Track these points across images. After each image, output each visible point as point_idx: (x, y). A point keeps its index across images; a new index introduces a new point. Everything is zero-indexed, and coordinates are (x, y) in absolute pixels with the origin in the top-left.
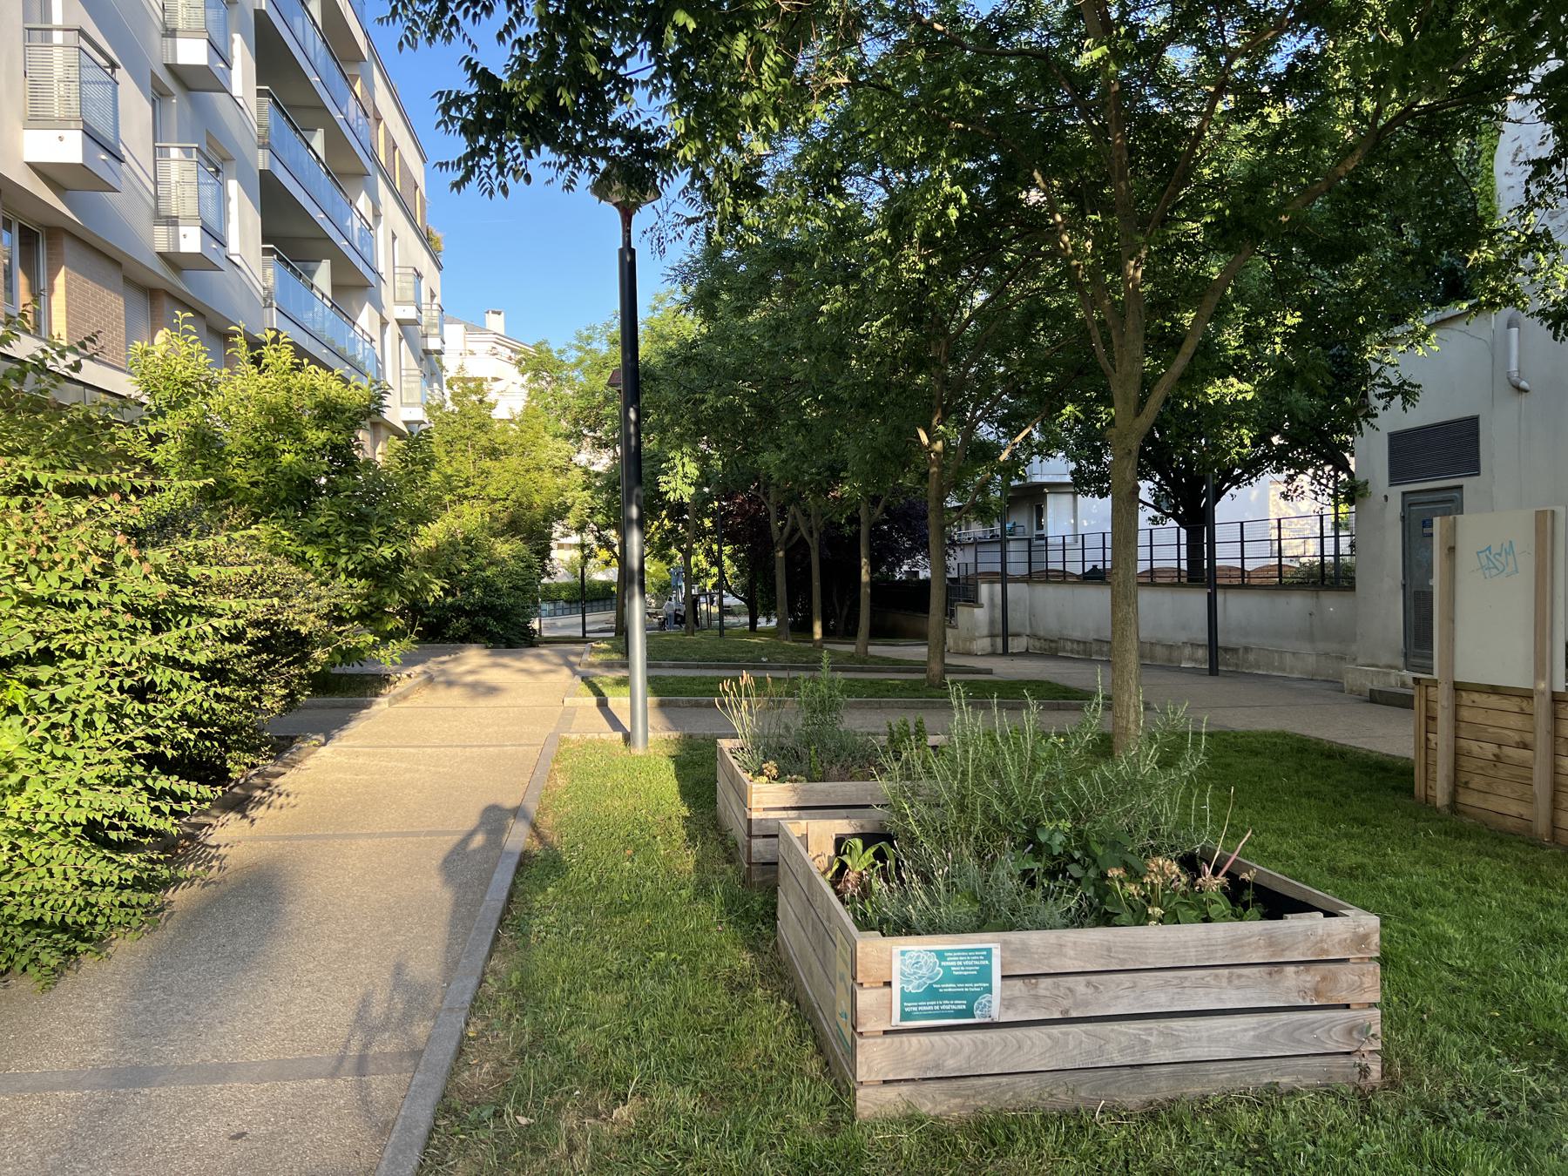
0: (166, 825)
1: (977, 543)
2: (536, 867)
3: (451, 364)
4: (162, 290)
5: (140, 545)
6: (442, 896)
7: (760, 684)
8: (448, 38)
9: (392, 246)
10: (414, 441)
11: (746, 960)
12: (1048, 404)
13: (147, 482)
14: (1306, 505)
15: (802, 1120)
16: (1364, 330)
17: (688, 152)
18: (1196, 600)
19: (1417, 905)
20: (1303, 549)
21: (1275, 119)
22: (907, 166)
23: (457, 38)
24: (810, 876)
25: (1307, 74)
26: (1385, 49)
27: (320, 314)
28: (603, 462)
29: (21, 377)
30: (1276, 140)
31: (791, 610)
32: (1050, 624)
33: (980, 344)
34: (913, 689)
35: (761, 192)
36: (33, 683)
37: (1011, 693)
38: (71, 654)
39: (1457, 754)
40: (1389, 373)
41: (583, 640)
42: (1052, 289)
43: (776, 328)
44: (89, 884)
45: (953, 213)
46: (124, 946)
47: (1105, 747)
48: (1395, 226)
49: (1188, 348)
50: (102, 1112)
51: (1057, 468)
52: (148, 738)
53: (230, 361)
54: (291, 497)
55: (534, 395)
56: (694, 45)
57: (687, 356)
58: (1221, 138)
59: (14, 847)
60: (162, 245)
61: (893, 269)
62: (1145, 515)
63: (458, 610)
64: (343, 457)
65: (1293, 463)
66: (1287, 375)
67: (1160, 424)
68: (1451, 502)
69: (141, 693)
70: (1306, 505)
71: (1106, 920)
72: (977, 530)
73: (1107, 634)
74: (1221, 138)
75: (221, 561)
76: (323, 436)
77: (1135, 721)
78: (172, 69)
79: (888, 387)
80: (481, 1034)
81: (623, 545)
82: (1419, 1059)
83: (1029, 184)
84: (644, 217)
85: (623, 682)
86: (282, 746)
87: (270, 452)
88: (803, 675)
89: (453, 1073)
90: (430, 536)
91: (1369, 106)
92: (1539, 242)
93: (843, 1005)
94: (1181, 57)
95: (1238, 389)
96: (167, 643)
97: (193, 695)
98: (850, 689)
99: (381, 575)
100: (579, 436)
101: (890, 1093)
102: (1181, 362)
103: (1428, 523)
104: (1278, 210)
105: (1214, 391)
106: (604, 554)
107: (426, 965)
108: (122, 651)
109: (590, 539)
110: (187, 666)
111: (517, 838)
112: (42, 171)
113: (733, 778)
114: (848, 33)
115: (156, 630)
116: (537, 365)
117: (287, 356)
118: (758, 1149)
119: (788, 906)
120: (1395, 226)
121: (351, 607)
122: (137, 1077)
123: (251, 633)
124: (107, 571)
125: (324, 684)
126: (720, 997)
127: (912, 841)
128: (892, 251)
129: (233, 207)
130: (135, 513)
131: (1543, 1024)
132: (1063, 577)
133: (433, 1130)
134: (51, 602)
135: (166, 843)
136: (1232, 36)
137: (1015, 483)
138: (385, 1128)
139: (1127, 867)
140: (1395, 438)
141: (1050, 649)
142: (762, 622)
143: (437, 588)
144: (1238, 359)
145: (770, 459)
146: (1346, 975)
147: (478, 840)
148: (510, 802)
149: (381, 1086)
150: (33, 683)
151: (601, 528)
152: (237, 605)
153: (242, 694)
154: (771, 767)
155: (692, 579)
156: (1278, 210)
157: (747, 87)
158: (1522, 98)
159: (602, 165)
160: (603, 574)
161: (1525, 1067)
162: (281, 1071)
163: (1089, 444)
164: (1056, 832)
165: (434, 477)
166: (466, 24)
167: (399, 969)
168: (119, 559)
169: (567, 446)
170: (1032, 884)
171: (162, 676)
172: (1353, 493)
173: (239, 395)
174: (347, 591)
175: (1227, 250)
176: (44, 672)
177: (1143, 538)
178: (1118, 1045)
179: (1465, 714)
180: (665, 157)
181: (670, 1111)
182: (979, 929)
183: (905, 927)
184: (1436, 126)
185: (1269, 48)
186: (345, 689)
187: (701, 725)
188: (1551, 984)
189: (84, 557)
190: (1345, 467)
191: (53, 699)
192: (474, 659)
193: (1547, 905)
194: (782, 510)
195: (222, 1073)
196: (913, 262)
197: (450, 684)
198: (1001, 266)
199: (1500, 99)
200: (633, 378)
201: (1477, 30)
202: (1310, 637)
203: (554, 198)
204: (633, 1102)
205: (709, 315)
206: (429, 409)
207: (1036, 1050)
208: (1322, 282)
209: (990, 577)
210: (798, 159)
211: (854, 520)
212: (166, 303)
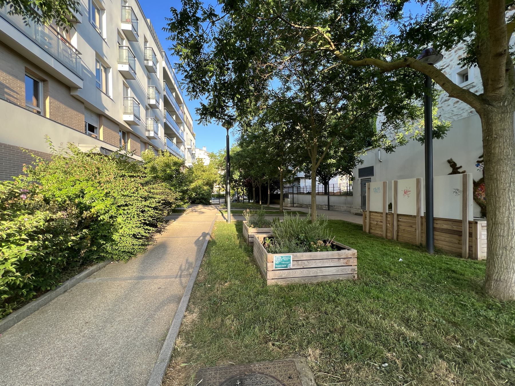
0: (147, 235)
1: (288, 187)
2: (211, 243)
3: (197, 156)
4: (147, 143)
5: (143, 186)
6: (195, 248)
7: (250, 211)
8: (197, 99)
9: (186, 135)
10: (190, 169)
11: (248, 258)
12: (300, 163)
13: (144, 175)
14: (345, 181)
15: (258, 285)
16: (354, 151)
17: (238, 119)
18: (326, 197)
19: (363, 249)
20: (344, 189)
21: (339, 115)
22: (276, 122)
23: (199, 99)
24: (259, 244)
25: (344, 107)
26: (357, 103)
27: (174, 147)
28: (223, 173)
29: (122, 157)
30: (339, 119)
31: (256, 199)
32: (301, 202)
33: (289, 153)
34: (277, 213)
35: (251, 126)
36: (124, 210)
37: (294, 213)
38: (131, 205)
39: (370, 223)
40: (358, 158)
41: (219, 204)
42: (301, 143)
43: (253, 149)
44: (133, 245)
45: (284, 130)
46: (139, 255)
47: (310, 222)
48: (359, 133)
49: (324, 154)
50: (135, 284)
51: (302, 174)
52: (144, 220)
53: (158, 155)
54: (168, 178)
55: (211, 161)
56: (240, 100)
57: (238, 154)
58: (330, 118)
59: (120, 238)
60: (147, 135)
61: (274, 139)
62: (317, 183)
63: (197, 198)
64: (177, 171)
65: (342, 174)
66: (341, 158)
67: (320, 167)
68: (369, 180)
69: (143, 212)
70: (345, 181)
71: (310, 251)
72: (288, 185)
73: (311, 203)
74: (330, 118)
75: (157, 189)
76: (174, 168)
77: (315, 218)
78: (149, 105)
79: (273, 160)
80: (202, 271)
81: (226, 187)
82: (364, 275)
83: (297, 125)
84: (230, 130)
85: (227, 211)
86: (167, 222)
87: (165, 171)
88: (258, 210)
89: (197, 277)
90: (193, 185)
91: (355, 113)
92: (384, 136)
93: (265, 266)
94: (323, 104)
95: (333, 161)
96: (147, 203)
97: (152, 212)
98: (266, 212)
99: (184, 192)
100: (219, 168)
101: (273, 281)
102: (323, 156)
103: (365, 184)
104: (340, 130)
105: (329, 161)
106: (223, 189)
107: (192, 259)
108: (139, 204)
109: (220, 186)
110: (151, 207)
111: (208, 238)
112: (126, 122)
113: (246, 228)
114: (266, 99)
115: (145, 201)
116: (212, 156)
117: (168, 154)
118: (250, 291)
119: (255, 249)
120: (359, 133)
121: (179, 198)
122: (142, 278)
123: (162, 202)
124: (137, 191)
125: (174, 211)
126: (244, 265)
127: (277, 238)
128: (273, 136)
129: (159, 128)
130: (142, 181)
131: (385, 269)
132: (303, 193)
133: (193, 287)
134: (127, 196)
135: (147, 238)
136: (332, 101)
137: (295, 177)
138: (184, 287)
139: (314, 242)
140: (360, 170)
141: (301, 206)
142: (251, 201)
143: (194, 194)
144: (333, 156)
145: (252, 172)
146: (351, 260)
147: (201, 238)
148: (207, 232)
149: (184, 280)
150: (124, 210)
151: (223, 184)
152: (159, 197)
153: (160, 212)
154: (252, 226)
155: (238, 194)
156: (340, 130)
157: (249, 108)
158: (381, 112)
159: (224, 121)
160: (223, 193)
161: (382, 276)
162: (166, 277)
163: (307, 170)
164: (302, 236)
165: (194, 175)
166: (201, 96)
167: (187, 260)
168: (139, 188)
169: (217, 170)
170: (298, 245)
171: (146, 209)
172: (352, 179)
173: (160, 161)
174: (178, 195)
175: (331, 137)
176: (126, 208)
177: (317, 187)
178: (312, 272)
179: (371, 217)
180: (235, 120)
181: (235, 284)
182: (289, 252)
183: (276, 252)
184: (366, 116)
185: (338, 103)
186: (177, 212)
187: (240, 219)
188: (386, 262)
189: (133, 188)
190: (351, 175)
191: (127, 213)
192: (200, 207)
193: (385, 249)
194: (254, 182)
195: (156, 277)
196: (277, 138)
197: (196, 211)
198: (292, 140)
199: (377, 112)
200: (229, 158)
201: (373, 100)
202: (345, 204)
203: (215, 125)
204: (228, 282)
205: (242, 147)
206: (193, 164)
207: (298, 273)
208: (347, 143)
209: (291, 193)
210: (257, 121)
211: (267, 183)
212: (148, 145)
